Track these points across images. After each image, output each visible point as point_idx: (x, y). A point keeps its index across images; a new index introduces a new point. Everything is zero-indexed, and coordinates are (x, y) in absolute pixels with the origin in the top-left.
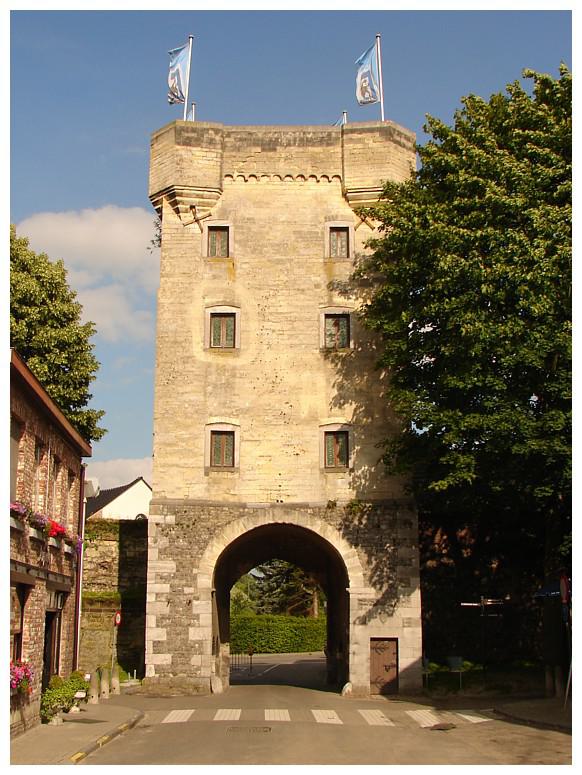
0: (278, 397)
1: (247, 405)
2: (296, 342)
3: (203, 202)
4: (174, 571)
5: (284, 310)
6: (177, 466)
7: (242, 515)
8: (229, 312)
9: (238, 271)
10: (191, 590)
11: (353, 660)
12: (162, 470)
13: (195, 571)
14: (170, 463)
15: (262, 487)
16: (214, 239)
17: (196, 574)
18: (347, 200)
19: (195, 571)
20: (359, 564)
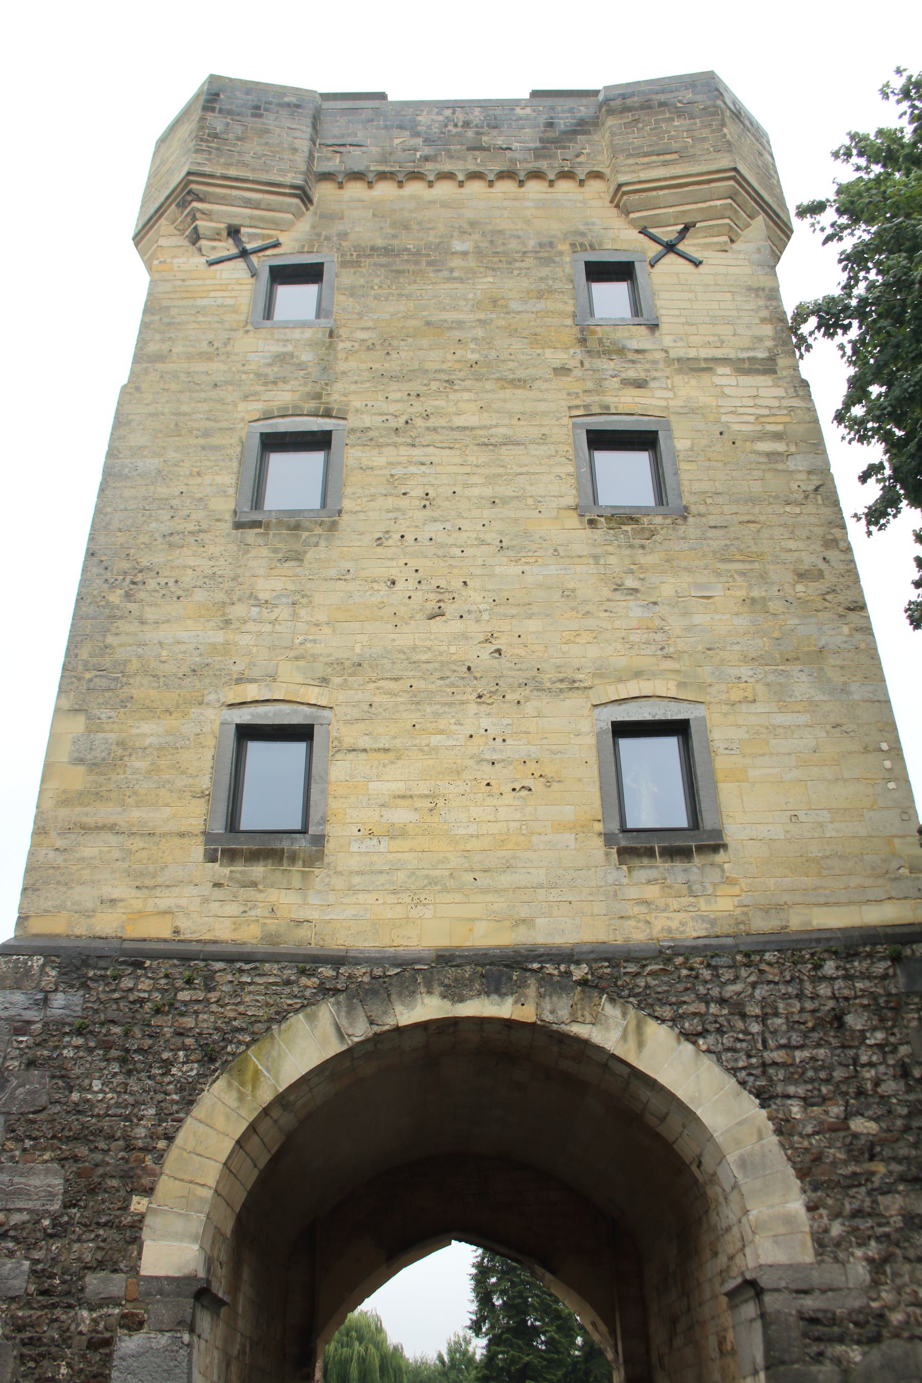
0: (457, 626)
1: (358, 649)
2: (508, 491)
3: (262, 219)
4: (56, 1206)
5: (473, 420)
6: (112, 828)
7: (326, 991)
8: (296, 720)
9: (341, 346)
10: (117, 1284)
11: (339, 102)
12: (59, 843)
13: (138, 1204)
14: (90, 821)
15: (362, 516)
16: (246, 547)
17: (143, 1216)
18: (625, 211)
19: (138, 1204)
20: (807, 1229)
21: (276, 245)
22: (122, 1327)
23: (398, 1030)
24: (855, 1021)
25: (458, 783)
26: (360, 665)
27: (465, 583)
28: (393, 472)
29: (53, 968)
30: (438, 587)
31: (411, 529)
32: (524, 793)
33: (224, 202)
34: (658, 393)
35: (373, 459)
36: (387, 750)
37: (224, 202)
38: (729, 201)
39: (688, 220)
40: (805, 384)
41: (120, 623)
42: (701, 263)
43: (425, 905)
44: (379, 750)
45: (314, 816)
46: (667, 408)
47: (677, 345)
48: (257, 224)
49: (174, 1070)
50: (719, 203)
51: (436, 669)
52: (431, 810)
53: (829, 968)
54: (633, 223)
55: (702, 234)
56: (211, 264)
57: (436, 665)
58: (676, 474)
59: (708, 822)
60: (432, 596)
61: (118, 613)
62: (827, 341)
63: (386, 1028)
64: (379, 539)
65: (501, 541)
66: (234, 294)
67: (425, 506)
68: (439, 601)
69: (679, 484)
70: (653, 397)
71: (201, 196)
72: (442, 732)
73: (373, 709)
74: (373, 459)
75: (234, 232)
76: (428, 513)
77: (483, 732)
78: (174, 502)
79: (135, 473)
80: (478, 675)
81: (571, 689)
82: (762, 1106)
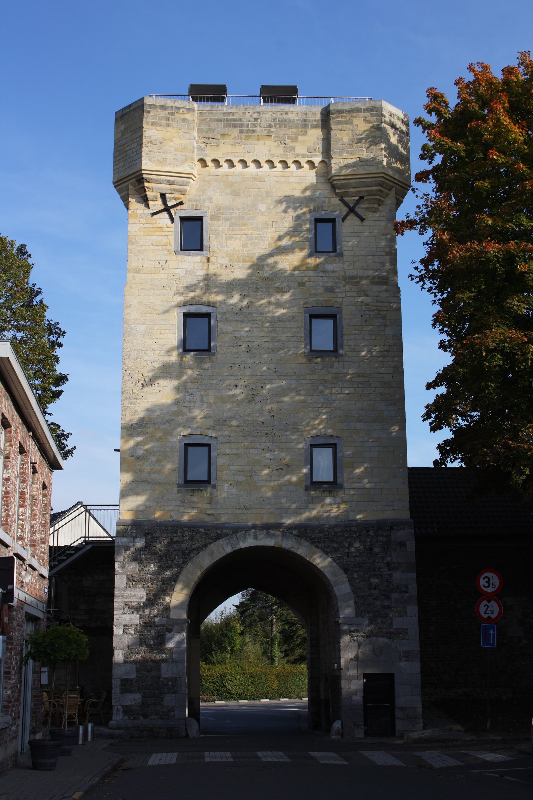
3: (175, 190)
21: (181, 203)
22: (167, 631)
23: (241, 550)
24: (376, 550)
25: (259, 467)
26: (225, 421)
27: (262, 387)
28: (235, 335)
29: (135, 530)
30: (252, 389)
31: (243, 362)
32: (280, 470)
33: (158, 182)
34: (339, 295)
35: (228, 328)
36: (236, 454)
37: (158, 182)
38: (380, 188)
39: (362, 195)
40: (399, 288)
41: (139, 401)
42: (364, 219)
43: (248, 509)
44: (233, 454)
45: (213, 477)
46: (342, 302)
47: (350, 268)
48: (173, 192)
49: (175, 562)
50: (375, 188)
51: (251, 423)
52: (250, 476)
53: (371, 533)
54: (337, 194)
55: (366, 203)
56: (153, 214)
57: (252, 422)
58: (342, 336)
59: (339, 480)
60: (251, 393)
61: (138, 397)
62: (431, 189)
63: (237, 549)
64: (231, 366)
65: (275, 369)
66: (165, 233)
67: (247, 352)
68: (253, 395)
69: (342, 341)
70: (337, 297)
71: (148, 180)
72: (253, 448)
73: (230, 439)
74: (228, 328)
75: (163, 196)
76: (248, 354)
77: (267, 448)
78: (153, 347)
79: (136, 332)
80: (266, 426)
81: (297, 432)
82: (345, 573)
